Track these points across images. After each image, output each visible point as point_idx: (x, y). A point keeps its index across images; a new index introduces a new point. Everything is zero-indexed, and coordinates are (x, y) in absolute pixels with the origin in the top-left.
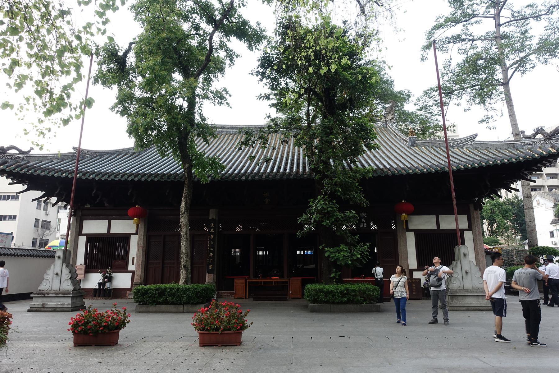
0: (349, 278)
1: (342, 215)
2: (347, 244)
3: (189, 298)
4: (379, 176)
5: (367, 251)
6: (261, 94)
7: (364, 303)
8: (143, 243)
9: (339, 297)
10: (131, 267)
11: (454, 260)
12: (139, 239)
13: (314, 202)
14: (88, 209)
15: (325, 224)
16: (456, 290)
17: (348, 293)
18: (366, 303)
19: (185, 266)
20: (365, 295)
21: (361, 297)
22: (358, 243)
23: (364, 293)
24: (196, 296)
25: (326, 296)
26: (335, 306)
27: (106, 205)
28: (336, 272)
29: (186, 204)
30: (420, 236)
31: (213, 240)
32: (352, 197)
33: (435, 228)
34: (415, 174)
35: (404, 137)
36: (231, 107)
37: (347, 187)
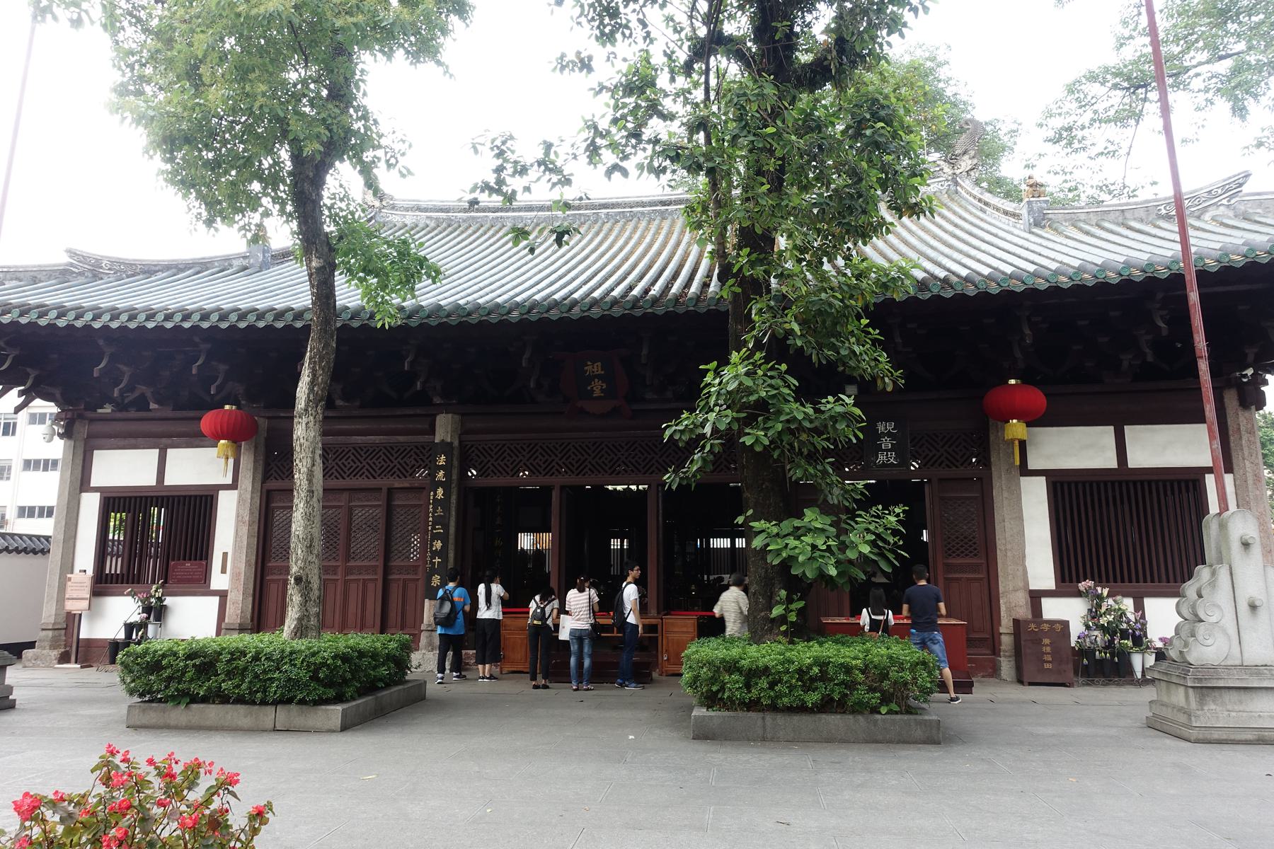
0: (840, 615)
1: (810, 411)
2: (826, 509)
3: (292, 683)
4: (938, 298)
5: (895, 532)
6: (563, 56)
7: (884, 710)
8: (251, 513)
9: (791, 688)
10: (219, 580)
11: (1204, 563)
12: (241, 500)
13: (717, 373)
14: (105, 419)
15: (748, 441)
16: (1214, 668)
17: (823, 677)
18: (890, 712)
19: (298, 580)
20: (886, 685)
21: (872, 690)
22: (865, 504)
23: (884, 676)
24: (314, 678)
25: (748, 686)
26: (781, 719)
27: (153, 406)
28: (789, 600)
29: (312, 383)
30: (1067, 490)
31: (444, 503)
32: (843, 352)
33: (1112, 463)
34: (1055, 291)
35: (1009, 206)
36: (451, 76)
37: (823, 322)
